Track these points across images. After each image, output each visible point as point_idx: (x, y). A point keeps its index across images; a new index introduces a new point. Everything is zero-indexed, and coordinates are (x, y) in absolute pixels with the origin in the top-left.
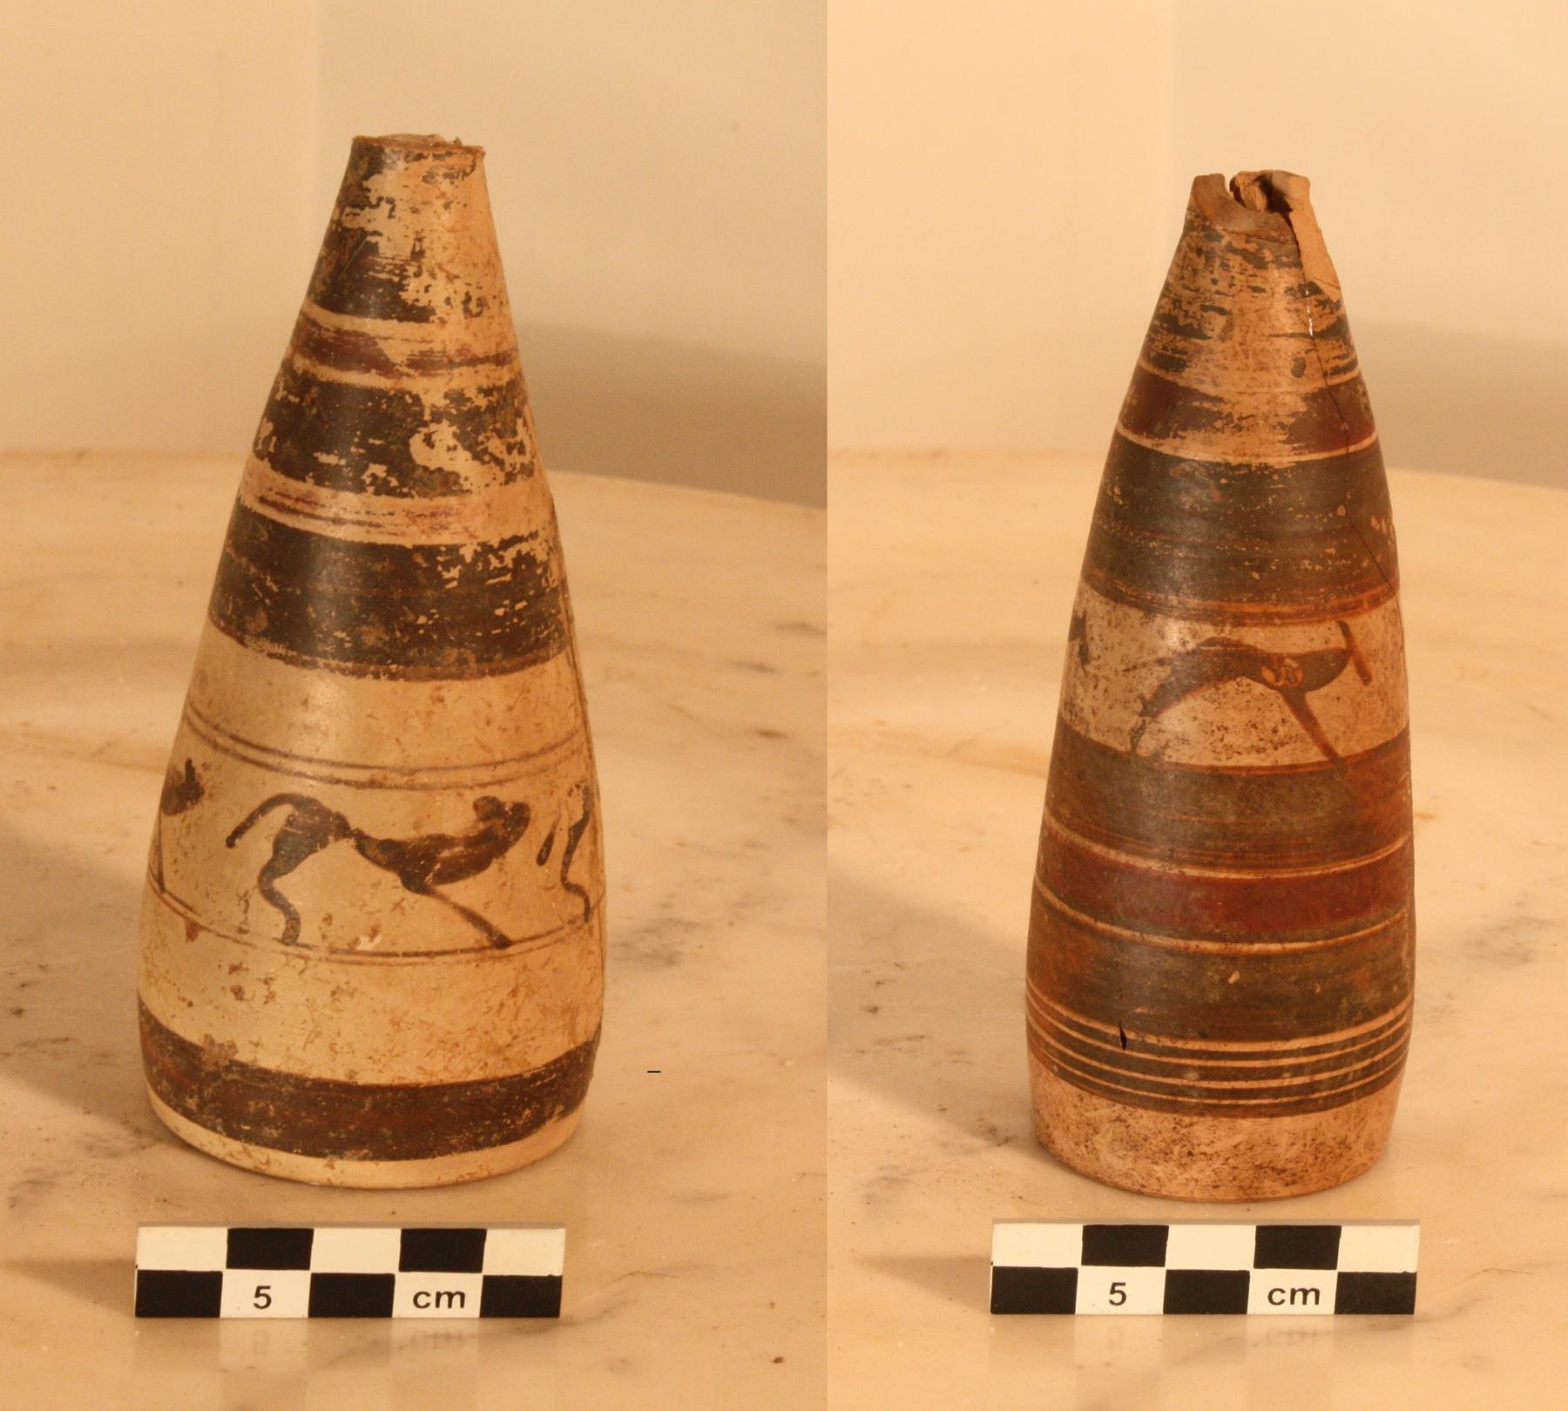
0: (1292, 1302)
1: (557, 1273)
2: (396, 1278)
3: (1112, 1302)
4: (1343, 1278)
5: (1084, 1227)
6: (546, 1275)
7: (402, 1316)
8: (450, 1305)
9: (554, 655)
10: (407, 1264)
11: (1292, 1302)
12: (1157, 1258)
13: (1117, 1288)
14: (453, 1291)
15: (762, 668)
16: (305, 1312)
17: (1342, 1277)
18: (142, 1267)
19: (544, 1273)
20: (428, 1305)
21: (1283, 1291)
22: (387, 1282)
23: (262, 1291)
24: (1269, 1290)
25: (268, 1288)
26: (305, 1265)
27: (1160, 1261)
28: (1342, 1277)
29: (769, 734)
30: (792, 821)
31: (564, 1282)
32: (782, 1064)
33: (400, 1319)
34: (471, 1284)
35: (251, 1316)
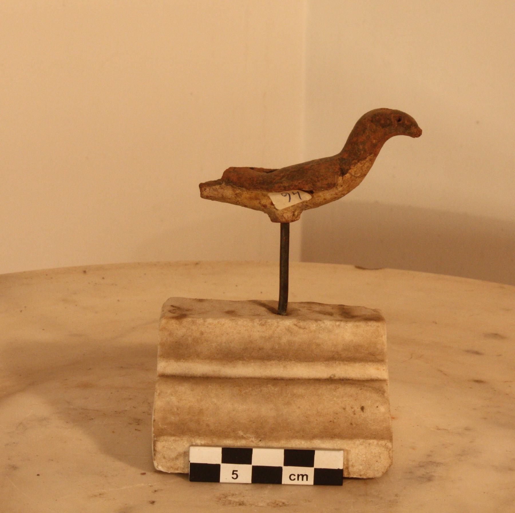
0: (298, 480)
2: (283, 468)
3: (233, 478)
4: (316, 470)
6: (337, 468)
7: (286, 483)
8: (303, 480)
10: (286, 463)
11: (298, 480)
12: (248, 461)
13: (235, 472)
15: (477, 353)
19: (336, 467)
20: (295, 479)
21: (294, 475)
22: (279, 470)
23: (235, 472)
24: (238, 477)
25: (237, 471)
26: (250, 463)
27: (250, 463)
29: (477, 381)
30: (485, 418)
34: (310, 471)
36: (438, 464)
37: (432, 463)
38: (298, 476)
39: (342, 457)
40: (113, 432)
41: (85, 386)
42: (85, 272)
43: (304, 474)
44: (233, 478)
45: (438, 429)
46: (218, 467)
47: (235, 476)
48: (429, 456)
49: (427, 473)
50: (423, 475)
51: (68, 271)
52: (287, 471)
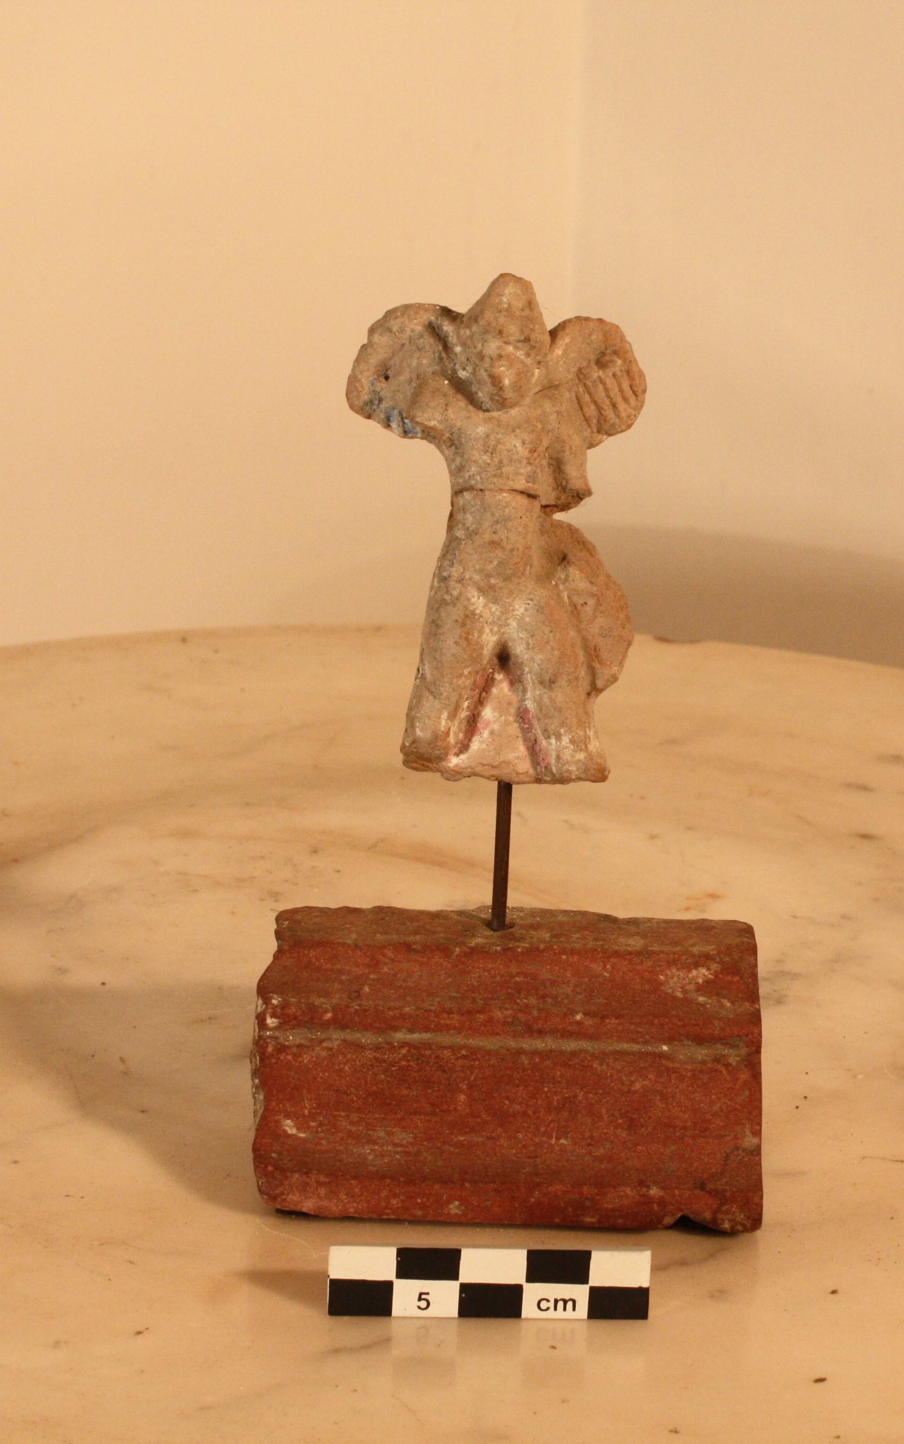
0: (555, 1309)
1: (645, 1285)
3: (419, 1307)
5: (401, 1253)
6: (637, 1286)
7: (529, 1316)
8: (565, 1309)
9: (261, 1019)
10: (532, 1277)
11: (555, 1309)
13: (423, 1297)
14: (567, 1298)
15: (864, 788)
16: (455, 1313)
17: (592, 1289)
18: (334, 1276)
19: (635, 1285)
20: (548, 1309)
21: (548, 1301)
22: (517, 1291)
23: (423, 1297)
25: (428, 1294)
26: (455, 1277)
27: (455, 1277)
28: (592, 1289)
29: (866, 837)
31: (650, 1289)
32: (855, 1077)
33: (527, 1319)
34: (580, 1293)
35: (415, 1315)
36: (794, 976)
37: (785, 974)
38: (556, 1301)
39: (648, 1263)
40: (233, 913)
41: (185, 834)
42: (184, 640)
43: (567, 1299)
44: (419, 1307)
45: (795, 917)
46: (387, 1287)
47: (423, 1304)
48: (779, 961)
49: (775, 991)
50: (769, 994)
51: (156, 638)
52: (532, 1293)
